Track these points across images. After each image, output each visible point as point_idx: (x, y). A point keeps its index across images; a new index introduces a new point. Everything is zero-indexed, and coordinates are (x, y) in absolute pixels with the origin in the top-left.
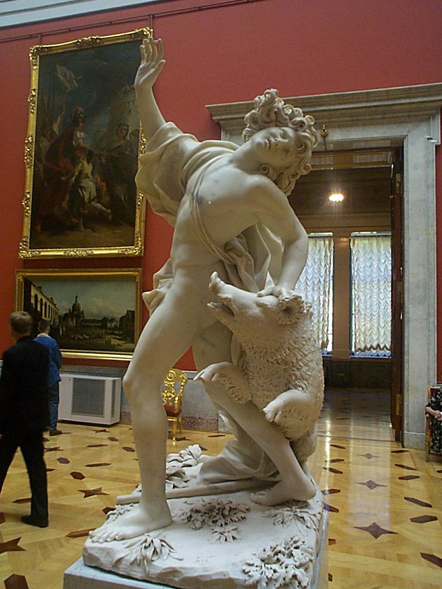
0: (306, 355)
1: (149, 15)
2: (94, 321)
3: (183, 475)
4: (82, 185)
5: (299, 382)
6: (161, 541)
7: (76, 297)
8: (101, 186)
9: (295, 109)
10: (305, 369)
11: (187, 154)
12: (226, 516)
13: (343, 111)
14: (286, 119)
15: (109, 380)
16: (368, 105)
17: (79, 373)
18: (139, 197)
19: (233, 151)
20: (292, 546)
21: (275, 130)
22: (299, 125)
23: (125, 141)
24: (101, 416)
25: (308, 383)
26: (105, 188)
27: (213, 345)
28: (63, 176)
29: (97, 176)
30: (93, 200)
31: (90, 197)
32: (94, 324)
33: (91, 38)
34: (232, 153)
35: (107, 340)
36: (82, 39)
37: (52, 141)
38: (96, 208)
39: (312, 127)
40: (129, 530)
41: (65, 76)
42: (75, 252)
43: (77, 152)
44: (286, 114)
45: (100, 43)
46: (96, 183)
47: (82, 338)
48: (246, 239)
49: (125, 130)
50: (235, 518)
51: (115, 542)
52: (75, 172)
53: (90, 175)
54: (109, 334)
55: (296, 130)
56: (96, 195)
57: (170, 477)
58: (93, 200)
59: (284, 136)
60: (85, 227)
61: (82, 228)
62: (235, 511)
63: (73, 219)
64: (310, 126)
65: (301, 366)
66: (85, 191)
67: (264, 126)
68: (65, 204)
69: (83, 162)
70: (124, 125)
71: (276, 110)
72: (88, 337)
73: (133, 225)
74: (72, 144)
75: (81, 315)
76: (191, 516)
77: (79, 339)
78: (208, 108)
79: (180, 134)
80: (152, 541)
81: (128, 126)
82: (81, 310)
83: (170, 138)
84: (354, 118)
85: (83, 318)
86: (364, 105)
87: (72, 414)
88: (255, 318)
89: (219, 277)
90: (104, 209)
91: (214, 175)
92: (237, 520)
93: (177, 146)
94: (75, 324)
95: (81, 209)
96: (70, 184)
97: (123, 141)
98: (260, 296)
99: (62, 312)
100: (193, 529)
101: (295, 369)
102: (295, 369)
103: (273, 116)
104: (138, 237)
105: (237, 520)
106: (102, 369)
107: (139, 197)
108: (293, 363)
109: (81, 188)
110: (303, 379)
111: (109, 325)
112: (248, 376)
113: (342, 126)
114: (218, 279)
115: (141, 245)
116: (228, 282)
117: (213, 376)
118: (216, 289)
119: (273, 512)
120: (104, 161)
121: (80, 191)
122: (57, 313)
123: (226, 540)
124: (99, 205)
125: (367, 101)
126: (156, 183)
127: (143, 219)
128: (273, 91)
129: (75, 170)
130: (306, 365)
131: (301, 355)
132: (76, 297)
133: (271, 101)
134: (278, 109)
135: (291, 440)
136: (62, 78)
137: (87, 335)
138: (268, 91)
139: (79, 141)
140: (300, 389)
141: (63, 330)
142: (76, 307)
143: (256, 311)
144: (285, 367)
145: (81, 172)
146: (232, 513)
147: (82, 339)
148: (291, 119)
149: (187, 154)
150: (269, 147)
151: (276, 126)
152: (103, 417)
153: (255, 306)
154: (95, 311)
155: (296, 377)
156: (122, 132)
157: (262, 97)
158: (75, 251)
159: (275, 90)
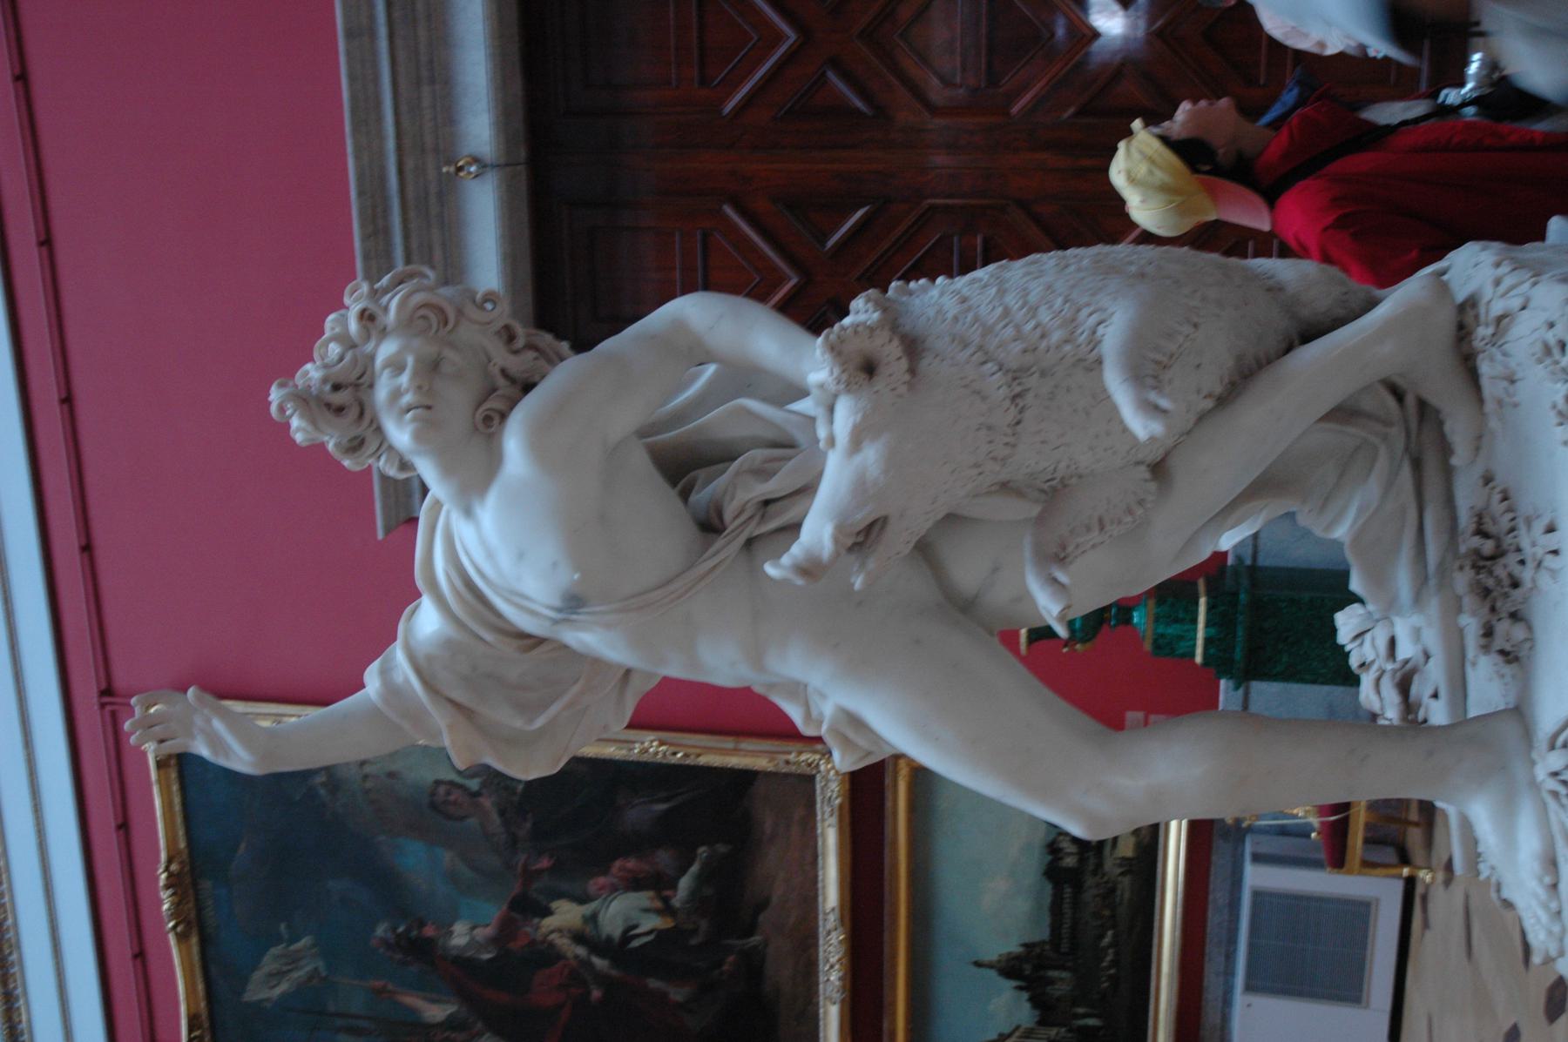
0: (1007, 312)
1: (103, 706)
2: (1056, 909)
3: (1408, 666)
4: (617, 933)
5: (1082, 333)
6: (1552, 747)
7: (978, 964)
8: (621, 874)
9: (327, 334)
10: (1044, 316)
11: (451, 631)
12: (1498, 546)
13: (404, 108)
14: (355, 361)
15: (1256, 877)
16: (382, 31)
17: (1229, 972)
18: (660, 755)
19: (445, 509)
20: (1557, 363)
21: (382, 393)
22: (369, 324)
23: (484, 791)
24: (1373, 907)
25: (1088, 305)
26: (631, 864)
27: (995, 570)
28: (589, 993)
29: (593, 885)
30: (666, 900)
31: (658, 912)
32: (1067, 908)
33: (167, 887)
34: (448, 512)
35: (1119, 871)
36: (166, 919)
37: (479, 1025)
38: (694, 893)
39: (377, 286)
40: (1529, 843)
41: (279, 975)
42: (832, 967)
43: (512, 946)
44: (341, 359)
45: (181, 863)
46: (614, 889)
47: (1111, 951)
48: (694, 469)
49: (448, 793)
50: (1504, 522)
51: (1562, 886)
52: (576, 957)
53: (587, 909)
54: (1100, 865)
55: (384, 333)
56: (651, 893)
57: (1409, 706)
58: (666, 900)
59: (397, 366)
60: (750, 930)
61: (756, 939)
62: (1487, 520)
63: (725, 968)
64: (375, 294)
65: (1035, 328)
66: (635, 927)
67: (372, 422)
68: (678, 994)
69: (544, 930)
70: (433, 794)
71: (328, 387)
72: (1110, 933)
73: (746, 778)
74: (490, 960)
75: (1038, 950)
76: (1503, 652)
77: (1114, 963)
78: (388, 530)
79: (398, 653)
80: (1555, 774)
81: (438, 783)
82: (1020, 950)
83: (407, 680)
84: (425, 73)
85: (1047, 947)
86: (383, 45)
87: (1367, 1006)
88: (893, 461)
89: (780, 557)
90: (695, 868)
91: (505, 560)
92: (1510, 515)
93: (430, 658)
94: (1064, 974)
95: (694, 942)
96: (614, 972)
97: (481, 800)
98: (832, 441)
99: (1025, 1014)
100: (1531, 648)
101: (1043, 345)
102: (1043, 345)
103: (338, 398)
104: (787, 762)
105: (1510, 515)
106: (1218, 894)
107: (660, 755)
108: (1025, 351)
109: (627, 937)
110: (1073, 320)
111: (1069, 862)
112: (1071, 477)
113: (447, 115)
114: (786, 560)
115: (815, 752)
116: (794, 528)
117: (1055, 580)
118: (810, 569)
119: (1490, 406)
120: (545, 863)
121: (636, 943)
122: (1029, 1034)
123: (1555, 552)
124: (685, 883)
125: (372, 34)
126: (531, 720)
127: (729, 743)
128: (275, 395)
129: (570, 954)
130: (1034, 311)
131: (1005, 326)
132: (978, 964)
133: (304, 400)
134: (325, 380)
135: (1297, 342)
136: (284, 987)
137: (1102, 936)
138: (274, 409)
139: (478, 938)
140: (1101, 330)
141: (1085, 1016)
142: (1010, 968)
143: (871, 454)
144: (1036, 375)
145: (579, 938)
146: (1489, 527)
147: (1117, 954)
148: (353, 346)
149: (451, 631)
150: (427, 411)
151: (371, 386)
152: (1377, 900)
153: (858, 459)
154: (1022, 906)
155: (1066, 341)
156: (455, 803)
157: (295, 422)
158: (827, 968)
159: (274, 389)
